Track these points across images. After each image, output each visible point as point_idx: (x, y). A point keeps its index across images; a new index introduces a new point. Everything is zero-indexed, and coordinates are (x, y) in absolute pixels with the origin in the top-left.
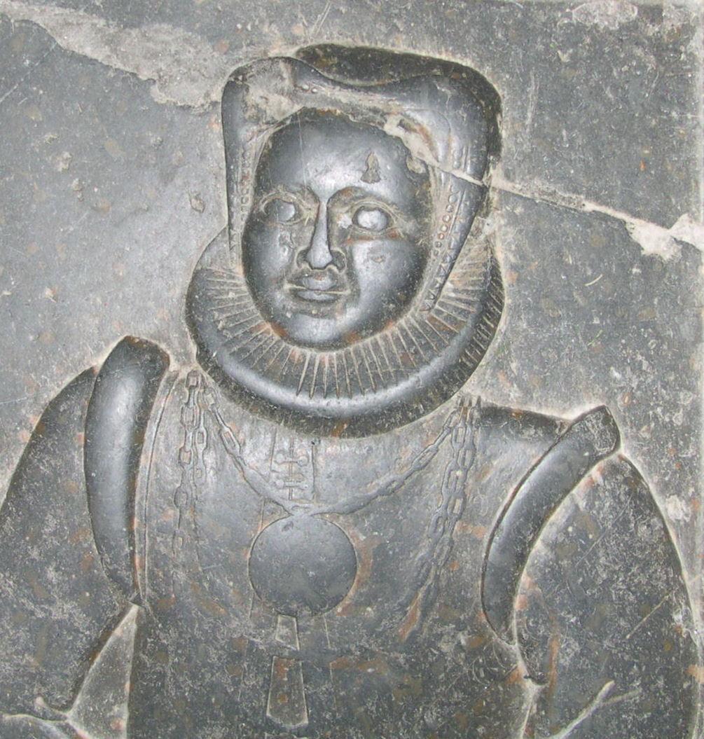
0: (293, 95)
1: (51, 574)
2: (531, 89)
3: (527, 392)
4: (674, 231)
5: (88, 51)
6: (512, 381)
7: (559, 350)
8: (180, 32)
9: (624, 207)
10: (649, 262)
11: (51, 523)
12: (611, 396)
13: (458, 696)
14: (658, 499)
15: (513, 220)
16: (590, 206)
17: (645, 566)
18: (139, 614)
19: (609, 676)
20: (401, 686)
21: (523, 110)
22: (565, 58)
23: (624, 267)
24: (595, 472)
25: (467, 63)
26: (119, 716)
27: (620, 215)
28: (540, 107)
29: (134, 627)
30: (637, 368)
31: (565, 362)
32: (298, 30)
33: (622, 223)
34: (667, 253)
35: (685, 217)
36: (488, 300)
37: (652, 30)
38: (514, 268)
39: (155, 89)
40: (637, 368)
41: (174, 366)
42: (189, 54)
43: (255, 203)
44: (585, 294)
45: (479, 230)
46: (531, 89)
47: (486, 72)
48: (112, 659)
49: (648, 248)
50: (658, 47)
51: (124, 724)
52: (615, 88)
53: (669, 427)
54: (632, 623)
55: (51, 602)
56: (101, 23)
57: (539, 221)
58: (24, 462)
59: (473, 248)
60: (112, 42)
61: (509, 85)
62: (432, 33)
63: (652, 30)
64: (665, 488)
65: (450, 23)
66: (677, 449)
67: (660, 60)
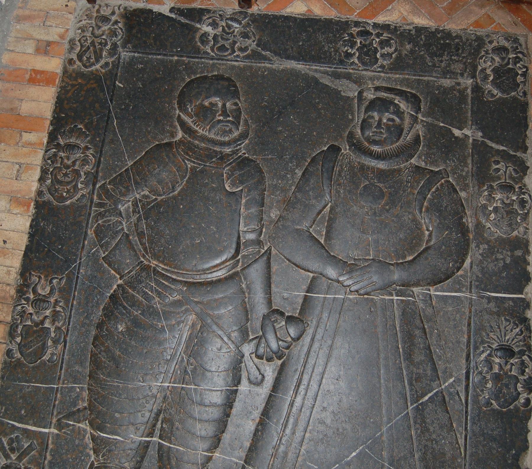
0: (374, 94)
1: (311, 193)
2: (429, 99)
3: (426, 164)
4: (463, 131)
5: (327, 83)
6: (423, 161)
7: (434, 155)
8: (348, 81)
9: (450, 125)
10: (456, 138)
11: (312, 181)
12: (447, 166)
13: (408, 231)
14: (459, 192)
15: (424, 126)
16: (442, 125)
17: (456, 205)
18: (331, 206)
19: (447, 230)
20: (395, 226)
21: (427, 102)
22: (437, 92)
23: (451, 139)
24: (443, 181)
25: (414, 92)
26: (323, 231)
27: (450, 127)
28: (431, 102)
29: (329, 209)
30: (454, 161)
31: (436, 158)
32: (375, 82)
33: (450, 129)
34: (461, 136)
35: (465, 129)
36: (417, 140)
37: (458, 87)
38: (423, 136)
39: (342, 92)
40: (454, 161)
41: (343, 151)
42: (350, 86)
43: (364, 117)
44: (441, 143)
45: (415, 127)
46: (429, 99)
47: (418, 94)
48: (323, 217)
49: (456, 135)
50: (459, 91)
51: (324, 233)
52: (449, 100)
53: (461, 175)
54: (453, 218)
55: (310, 200)
56: (330, 78)
57: (430, 127)
58: (306, 169)
59: (413, 131)
60: (333, 82)
61: (423, 97)
62: (406, 85)
63: (458, 87)
64: (461, 190)
65: (410, 83)
66: (464, 181)
67: (460, 94)
